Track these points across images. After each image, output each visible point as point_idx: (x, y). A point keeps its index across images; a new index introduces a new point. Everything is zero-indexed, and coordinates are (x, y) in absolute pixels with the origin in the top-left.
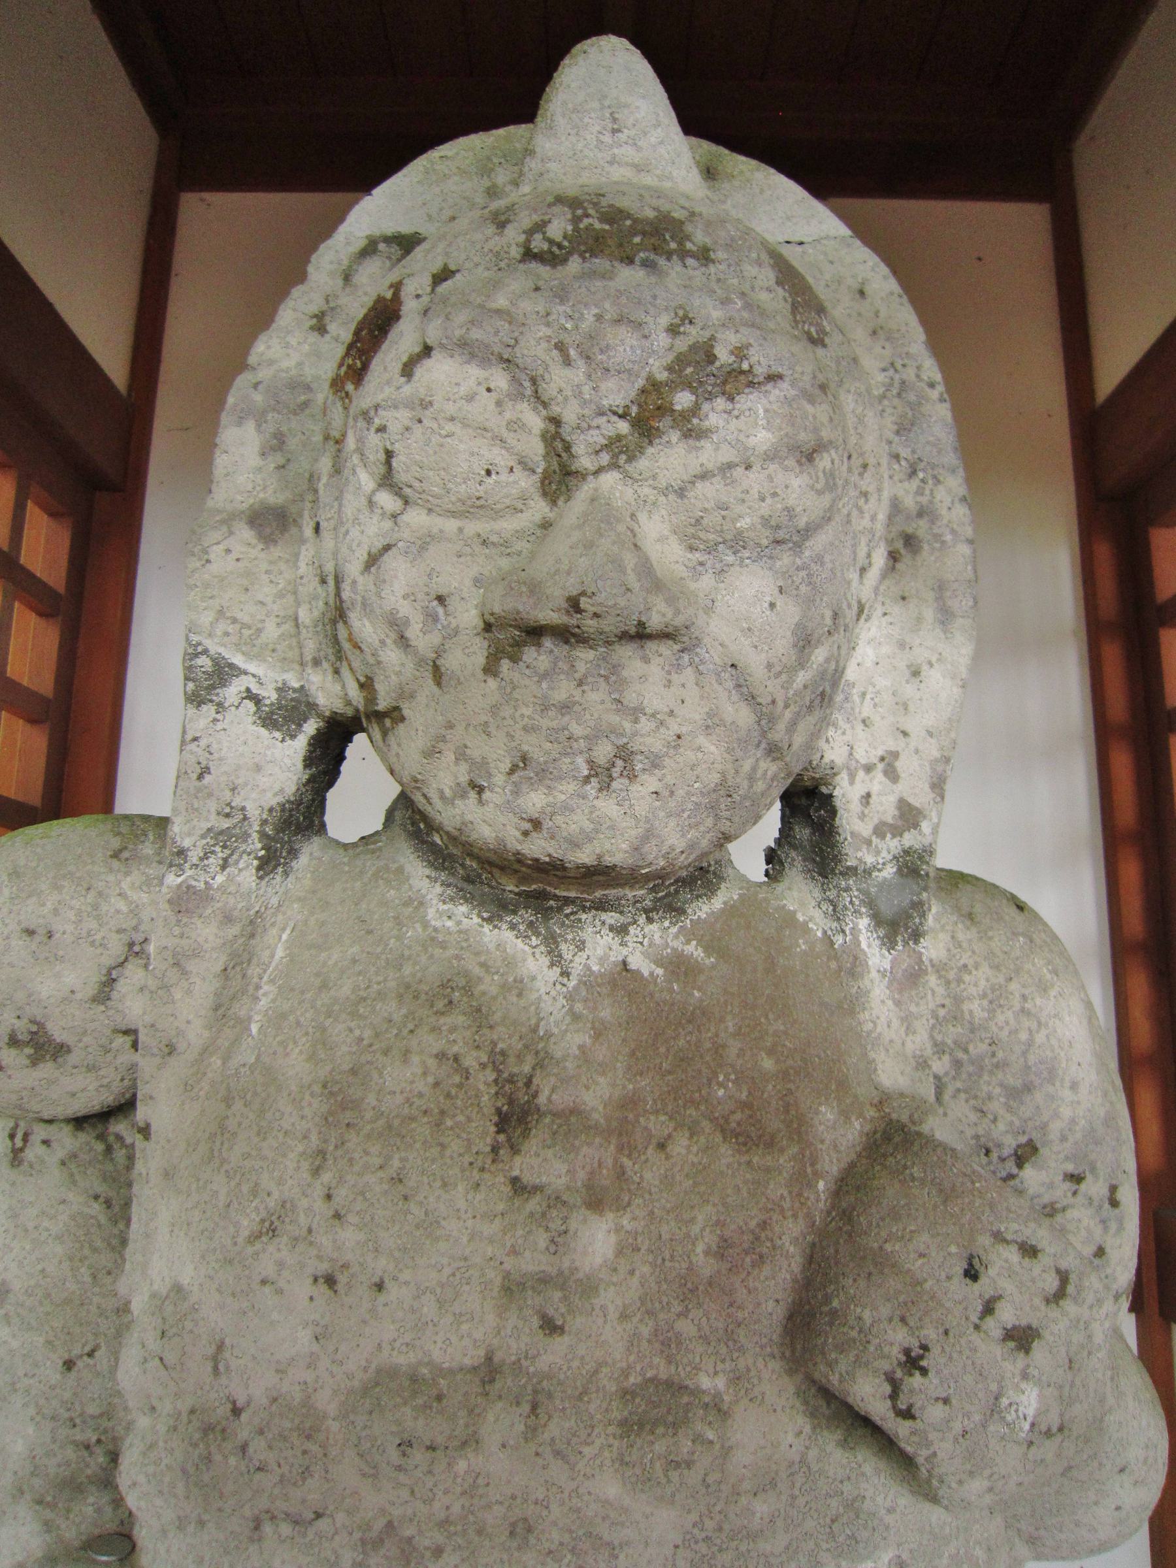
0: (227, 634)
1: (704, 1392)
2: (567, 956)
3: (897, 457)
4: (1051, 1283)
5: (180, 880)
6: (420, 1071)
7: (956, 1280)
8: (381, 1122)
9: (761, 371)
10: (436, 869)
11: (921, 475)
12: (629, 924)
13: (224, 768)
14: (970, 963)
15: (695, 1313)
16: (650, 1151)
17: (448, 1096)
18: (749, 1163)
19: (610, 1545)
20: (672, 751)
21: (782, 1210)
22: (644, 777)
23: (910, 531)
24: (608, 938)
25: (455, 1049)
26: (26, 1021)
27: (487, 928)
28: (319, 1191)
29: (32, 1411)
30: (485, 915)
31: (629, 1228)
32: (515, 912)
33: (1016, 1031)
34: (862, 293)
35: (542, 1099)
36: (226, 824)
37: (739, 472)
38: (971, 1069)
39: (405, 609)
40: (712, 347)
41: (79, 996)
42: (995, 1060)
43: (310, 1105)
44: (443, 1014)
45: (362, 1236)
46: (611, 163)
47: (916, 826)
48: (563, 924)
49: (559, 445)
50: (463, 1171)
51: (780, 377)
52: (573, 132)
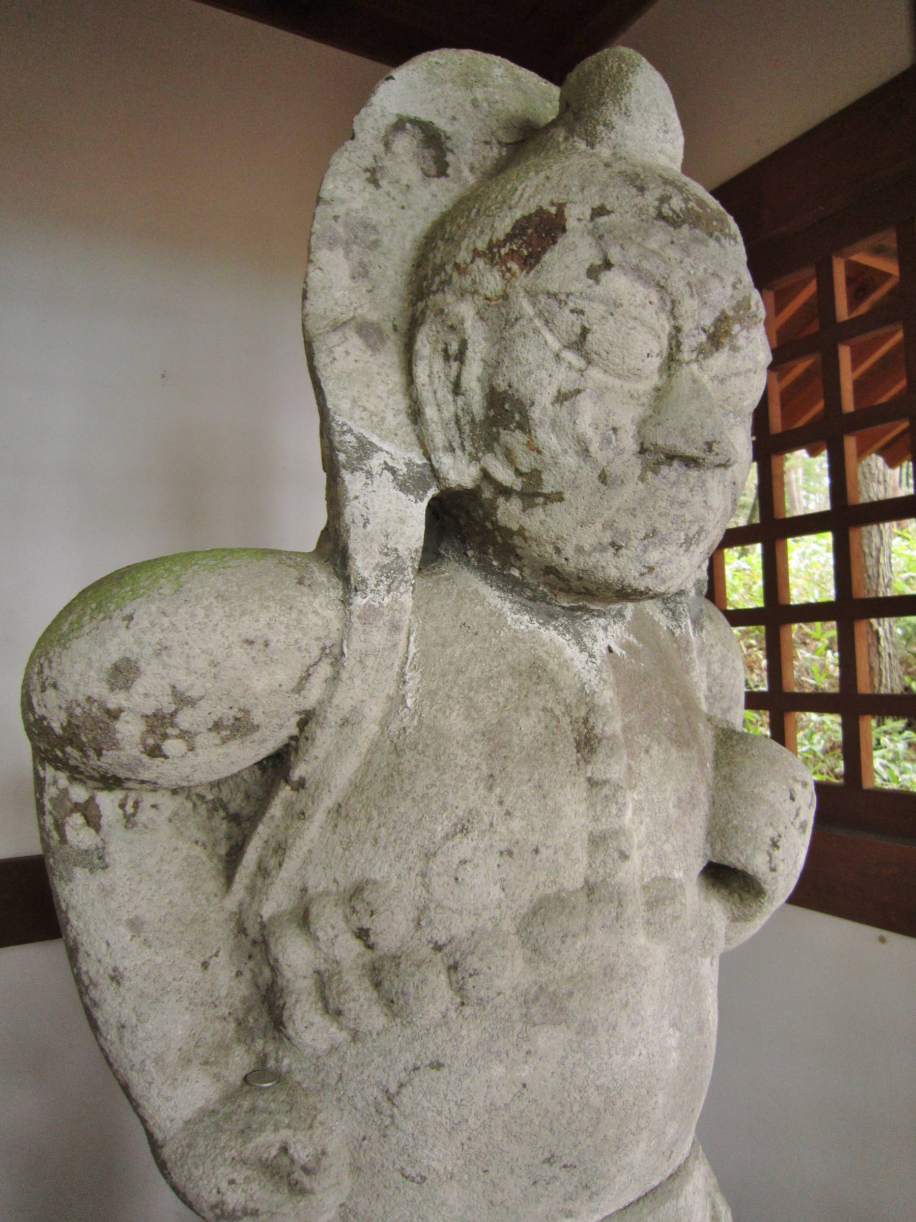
0: (362, 419)
2: (590, 645)
5: (365, 601)
6: (537, 720)
8: (524, 753)
10: (504, 591)
13: (378, 520)
16: (642, 755)
26: (236, 710)
27: (542, 630)
28: (493, 799)
29: (186, 1003)
30: (541, 621)
31: (637, 798)
32: (557, 619)
35: (597, 731)
36: (386, 561)
37: (751, 374)
39: (590, 433)
41: (284, 688)
43: (476, 747)
44: (538, 684)
45: (524, 823)
46: (660, 152)
48: (582, 626)
49: (674, 343)
52: (644, 125)
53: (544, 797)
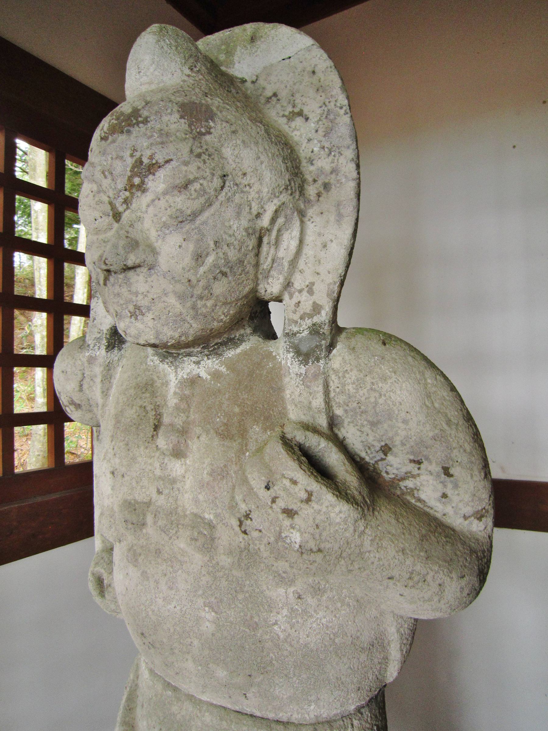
1: (205, 519)
3: (323, 148)
4: (304, 496)
7: (262, 489)
9: (161, 161)
11: (333, 153)
12: (201, 360)
14: (349, 369)
15: (203, 493)
17: (141, 419)
18: (223, 444)
19: (180, 561)
20: (153, 305)
21: (232, 462)
22: (147, 314)
23: (327, 181)
24: (193, 366)
25: (145, 404)
33: (369, 398)
34: (314, 72)
37: (157, 201)
38: (352, 413)
40: (141, 159)
42: (361, 410)
46: (141, 85)
47: (319, 313)
50: (143, 442)
51: (172, 160)
53: (129, 450)
